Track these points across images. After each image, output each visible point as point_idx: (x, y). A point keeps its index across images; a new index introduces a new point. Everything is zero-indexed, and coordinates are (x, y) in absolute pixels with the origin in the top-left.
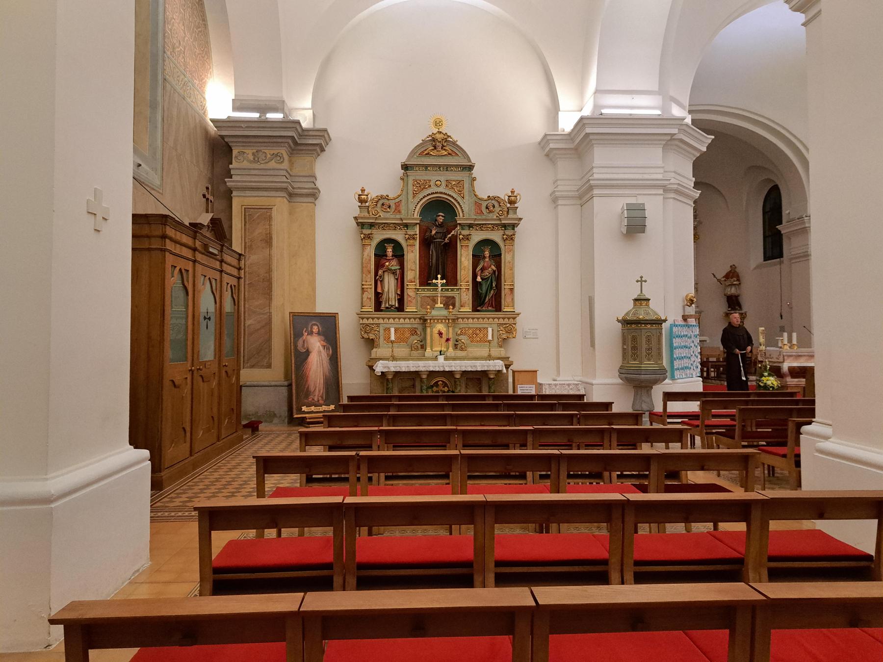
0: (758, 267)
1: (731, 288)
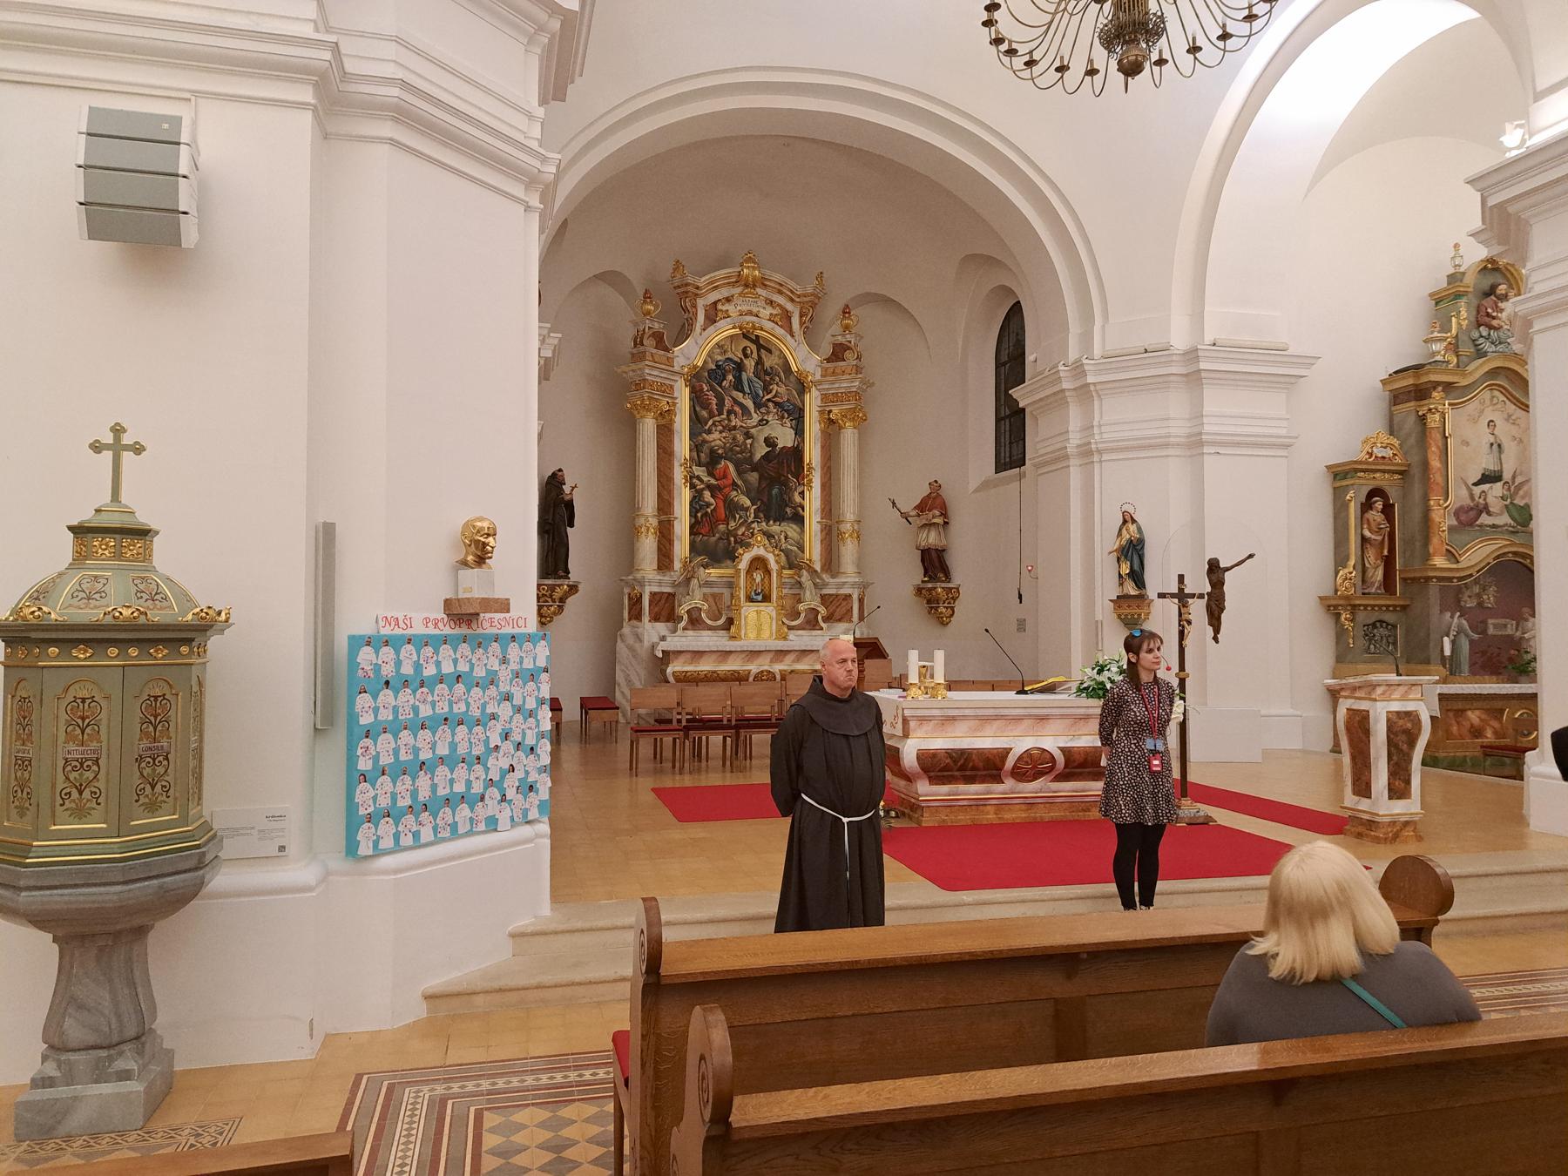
0: (985, 485)
1: (929, 532)
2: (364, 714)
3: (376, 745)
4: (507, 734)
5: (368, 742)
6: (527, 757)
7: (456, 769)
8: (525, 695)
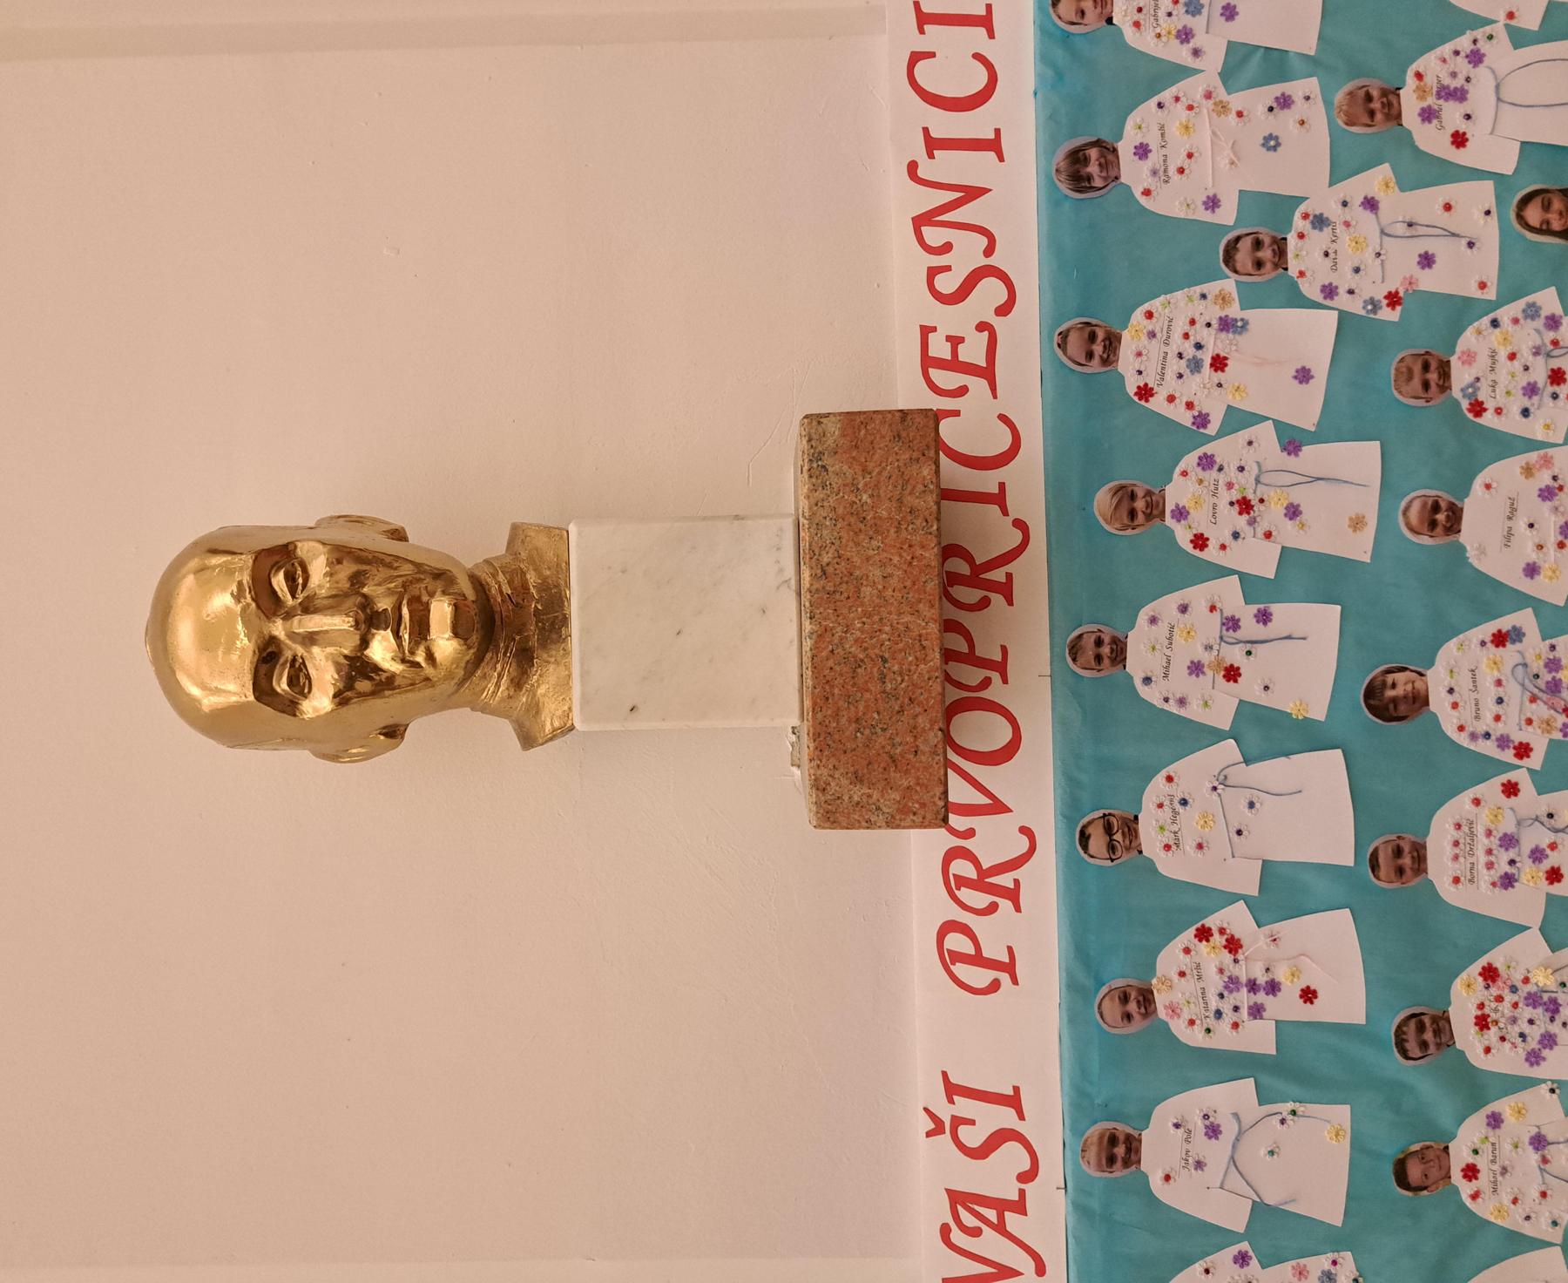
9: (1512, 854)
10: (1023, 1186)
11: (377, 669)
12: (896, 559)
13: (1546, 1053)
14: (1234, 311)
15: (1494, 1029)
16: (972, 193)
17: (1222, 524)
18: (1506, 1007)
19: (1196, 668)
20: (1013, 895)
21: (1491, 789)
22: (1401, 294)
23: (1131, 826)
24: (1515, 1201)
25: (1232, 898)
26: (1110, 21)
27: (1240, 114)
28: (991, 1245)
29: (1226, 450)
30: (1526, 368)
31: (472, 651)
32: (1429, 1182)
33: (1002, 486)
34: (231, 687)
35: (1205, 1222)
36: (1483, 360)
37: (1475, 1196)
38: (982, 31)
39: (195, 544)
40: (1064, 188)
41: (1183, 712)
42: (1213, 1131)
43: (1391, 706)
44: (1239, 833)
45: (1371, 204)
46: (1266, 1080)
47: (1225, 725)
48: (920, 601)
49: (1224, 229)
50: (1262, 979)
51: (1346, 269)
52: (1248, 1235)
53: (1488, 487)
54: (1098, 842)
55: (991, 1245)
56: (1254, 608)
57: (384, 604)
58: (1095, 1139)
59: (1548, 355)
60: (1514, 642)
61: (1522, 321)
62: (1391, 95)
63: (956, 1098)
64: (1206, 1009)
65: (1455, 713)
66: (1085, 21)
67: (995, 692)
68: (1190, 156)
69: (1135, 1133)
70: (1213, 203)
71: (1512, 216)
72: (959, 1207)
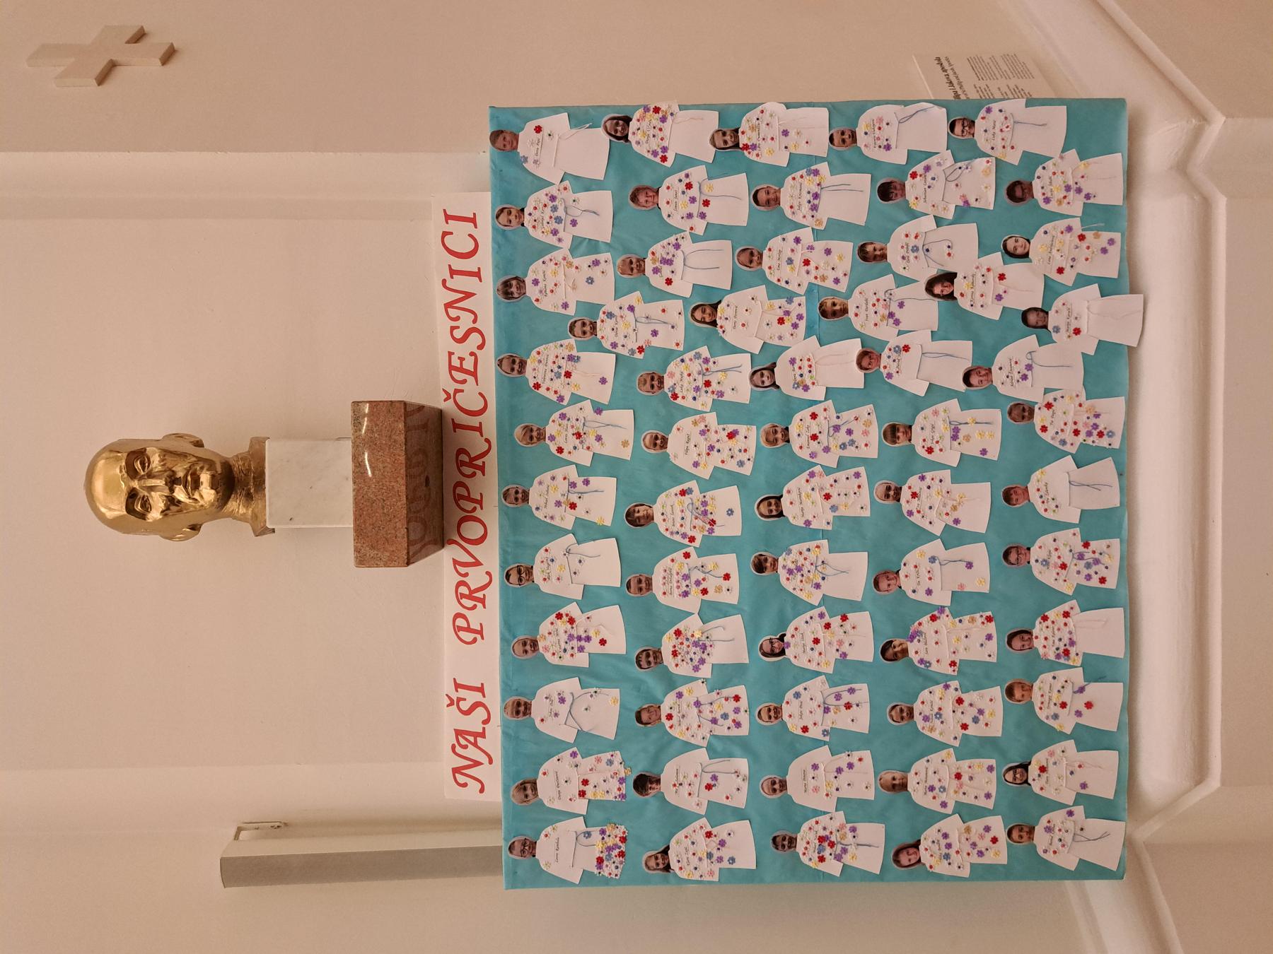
2: (726, 853)
3: (817, 813)
4: (824, 313)
5: (806, 836)
6: (914, 215)
7: (916, 519)
8: (700, 227)
9: (687, 582)
10: (484, 726)
11: (179, 502)
12: (388, 460)
13: (701, 666)
14: (574, 353)
15: (679, 657)
16: (468, 295)
17: (569, 443)
18: (684, 646)
19: (558, 504)
20: (482, 601)
21: (679, 555)
22: (644, 347)
23: (529, 571)
24: (688, 729)
25: (570, 601)
26: (523, 225)
27: (577, 268)
28: (472, 752)
29: (571, 411)
30: (695, 380)
31: (220, 494)
32: (650, 721)
33: (480, 423)
34: (116, 507)
35: (555, 738)
36: (678, 376)
37: (671, 727)
38: (472, 224)
39: (105, 448)
40: (501, 299)
41: (552, 523)
42: (562, 700)
43: (638, 521)
44: (575, 573)
45: (631, 308)
46: (583, 678)
47: (570, 527)
48: (398, 477)
49: (570, 317)
50: (583, 636)
51: (621, 336)
52: (575, 743)
53: (678, 429)
54: (514, 578)
55: (472, 752)
56: (582, 478)
57: (181, 474)
58: (511, 704)
59: (704, 375)
60: (688, 494)
61: (694, 360)
62: (641, 261)
63: (459, 689)
64: (560, 648)
65: (664, 523)
66: (512, 225)
67: (478, 514)
68: (556, 285)
69: (529, 701)
70: (565, 306)
71: (690, 315)
72: (459, 737)
